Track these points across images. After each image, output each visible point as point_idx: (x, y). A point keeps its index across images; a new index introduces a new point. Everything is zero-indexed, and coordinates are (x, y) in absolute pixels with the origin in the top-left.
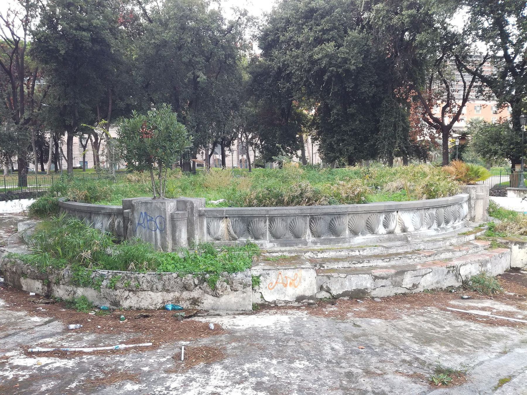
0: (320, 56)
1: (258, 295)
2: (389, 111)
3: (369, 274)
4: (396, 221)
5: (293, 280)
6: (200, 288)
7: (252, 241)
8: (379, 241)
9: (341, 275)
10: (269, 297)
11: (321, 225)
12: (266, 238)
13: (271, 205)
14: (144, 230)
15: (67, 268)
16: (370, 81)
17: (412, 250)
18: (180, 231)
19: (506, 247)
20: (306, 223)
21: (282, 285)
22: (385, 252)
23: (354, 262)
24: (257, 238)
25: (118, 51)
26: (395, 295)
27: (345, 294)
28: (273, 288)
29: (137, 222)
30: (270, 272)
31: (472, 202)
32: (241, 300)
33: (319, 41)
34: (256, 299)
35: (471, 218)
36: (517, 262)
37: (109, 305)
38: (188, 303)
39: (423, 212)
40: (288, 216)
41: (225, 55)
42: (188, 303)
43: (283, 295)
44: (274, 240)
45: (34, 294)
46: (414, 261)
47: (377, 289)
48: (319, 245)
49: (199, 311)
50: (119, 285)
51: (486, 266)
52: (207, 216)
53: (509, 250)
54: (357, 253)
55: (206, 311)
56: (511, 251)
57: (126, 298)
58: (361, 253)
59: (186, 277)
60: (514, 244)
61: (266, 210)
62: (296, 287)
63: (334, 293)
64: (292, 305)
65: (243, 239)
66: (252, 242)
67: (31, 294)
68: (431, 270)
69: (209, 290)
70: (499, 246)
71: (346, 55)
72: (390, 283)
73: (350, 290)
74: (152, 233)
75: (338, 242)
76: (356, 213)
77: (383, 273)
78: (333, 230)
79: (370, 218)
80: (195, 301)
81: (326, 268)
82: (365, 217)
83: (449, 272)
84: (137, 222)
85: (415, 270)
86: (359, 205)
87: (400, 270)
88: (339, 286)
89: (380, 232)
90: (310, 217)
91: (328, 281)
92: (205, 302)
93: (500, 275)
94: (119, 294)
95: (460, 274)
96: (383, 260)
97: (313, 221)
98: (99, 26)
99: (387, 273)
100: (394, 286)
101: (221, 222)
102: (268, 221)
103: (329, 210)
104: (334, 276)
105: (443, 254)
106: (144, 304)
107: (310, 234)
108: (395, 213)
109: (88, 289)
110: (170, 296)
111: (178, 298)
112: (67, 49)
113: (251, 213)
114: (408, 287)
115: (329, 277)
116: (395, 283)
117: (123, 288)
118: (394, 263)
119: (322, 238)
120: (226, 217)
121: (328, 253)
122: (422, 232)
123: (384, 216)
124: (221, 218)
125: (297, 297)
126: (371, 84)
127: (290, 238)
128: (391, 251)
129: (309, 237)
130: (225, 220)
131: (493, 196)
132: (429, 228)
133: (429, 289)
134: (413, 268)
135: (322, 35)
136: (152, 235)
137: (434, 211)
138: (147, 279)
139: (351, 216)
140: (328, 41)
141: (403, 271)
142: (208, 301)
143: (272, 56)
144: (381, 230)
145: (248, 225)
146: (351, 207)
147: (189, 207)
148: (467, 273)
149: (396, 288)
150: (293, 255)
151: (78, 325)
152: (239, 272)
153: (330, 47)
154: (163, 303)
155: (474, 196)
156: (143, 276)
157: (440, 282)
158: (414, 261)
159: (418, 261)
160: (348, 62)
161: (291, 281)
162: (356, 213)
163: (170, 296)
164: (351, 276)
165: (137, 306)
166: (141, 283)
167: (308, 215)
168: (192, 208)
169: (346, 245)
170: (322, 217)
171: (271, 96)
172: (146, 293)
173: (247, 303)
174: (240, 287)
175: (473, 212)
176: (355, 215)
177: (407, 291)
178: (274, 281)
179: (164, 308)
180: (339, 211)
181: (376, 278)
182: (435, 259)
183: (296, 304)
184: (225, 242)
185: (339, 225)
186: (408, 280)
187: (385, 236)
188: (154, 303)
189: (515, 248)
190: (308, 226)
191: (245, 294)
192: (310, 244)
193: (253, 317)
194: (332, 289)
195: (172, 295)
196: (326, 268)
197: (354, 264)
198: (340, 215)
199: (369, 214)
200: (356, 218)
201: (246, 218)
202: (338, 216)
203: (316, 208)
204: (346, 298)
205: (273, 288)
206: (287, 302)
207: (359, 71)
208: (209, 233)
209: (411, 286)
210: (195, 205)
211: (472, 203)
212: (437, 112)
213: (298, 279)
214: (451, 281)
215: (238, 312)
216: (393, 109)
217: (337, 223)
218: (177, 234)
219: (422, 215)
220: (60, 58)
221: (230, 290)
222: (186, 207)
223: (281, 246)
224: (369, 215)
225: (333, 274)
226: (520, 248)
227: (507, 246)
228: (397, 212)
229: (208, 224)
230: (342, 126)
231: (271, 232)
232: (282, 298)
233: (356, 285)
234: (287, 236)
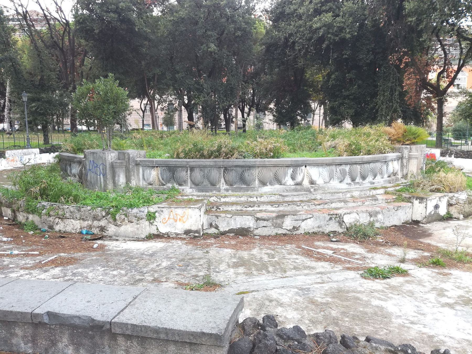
0: (318, 25)
1: (154, 228)
2: (387, 77)
3: (252, 216)
4: (303, 174)
5: (181, 217)
6: (106, 219)
7: (176, 186)
8: (286, 191)
9: (228, 215)
10: (163, 230)
11: (232, 176)
12: (188, 185)
13: (196, 158)
14: (92, 175)
15: (24, 199)
16: (368, 49)
17: (308, 199)
18: (119, 176)
19: (408, 202)
20: (220, 174)
21: (173, 220)
22: (281, 199)
23: (246, 206)
24: (180, 185)
25: (142, 29)
26: (275, 234)
27: (231, 231)
28: (166, 222)
29: (88, 168)
30: (163, 209)
31: (405, 161)
32: (136, 229)
33: (318, 12)
34: (153, 230)
35: (403, 176)
36: (417, 216)
37: (47, 228)
38: (98, 229)
39: (333, 167)
40: (205, 167)
41: (235, 29)
42: (98, 229)
43: (174, 229)
44: (194, 186)
45: (7, 218)
46: (302, 208)
47: (259, 229)
48: (230, 192)
49: (106, 237)
50: (52, 213)
51: (376, 216)
52: (142, 165)
53: (410, 204)
54: (255, 199)
55: (110, 237)
56: (413, 205)
57: (57, 224)
58: (259, 199)
59: (97, 210)
60: (415, 199)
61: (186, 161)
62: (184, 222)
63: (222, 230)
64: (181, 236)
65: (170, 185)
66: (177, 187)
67: (5, 218)
68: (311, 216)
69: (111, 220)
70: (403, 201)
71: (342, 25)
72: (271, 225)
73: (235, 228)
74: (98, 177)
75: (248, 191)
76: (264, 166)
77: (265, 216)
78: (242, 180)
79: (277, 171)
80: (102, 229)
81: (222, 210)
82: (274, 170)
83: (331, 219)
84: (88, 168)
85: (295, 215)
86: (266, 159)
87: (282, 213)
88: (226, 225)
89: (288, 184)
90: (224, 168)
91: (217, 220)
92: (109, 229)
93: (395, 226)
94: (52, 220)
95: (344, 222)
96: (272, 205)
97: (226, 172)
98: (124, 8)
99: (268, 215)
100: (275, 227)
101: (153, 170)
102: (189, 171)
103: (239, 163)
104: (222, 216)
105: (333, 204)
106: (69, 229)
107: (224, 183)
108: (303, 168)
109: (35, 215)
110: (85, 224)
111: (91, 226)
112: (101, 29)
113: (174, 163)
114: (288, 228)
115: (217, 217)
116: (276, 224)
117: (54, 216)
118: (283, 209)
119: (235, 186)
120: (157, 167)
121: (230, 198)
122: (331, 185)
123: (292, 170)
124: (153, 167)
125: (185, 231)
126: (368, 52)
127: (207, 185)
128: (287, 199)
129: (223, 186)
130: (156, 168)
131: (462, 158)
132: (341, 182)
133: (310, 232)
134: (294, 213)
135: (321, 7)
136: (98, 179)
137: (347, 168)
138: (70, 210)
139: (260, 169)
140: (327, 11)
141: (283, 215)
142: (112, 229)
143: (279, 27)
144: (289, 181)
145: (174, 174)
146: (258, 160)
147: (127, 157)
148: (352, 220)
149: (277, 229)
150: (200, 198)
151: (10, 239)
152: (136, 208)
153: (327, 17)
154: (81, 228)
155: (407, 156)
156: (68, 208)
157: (321, 227)
158: (302, 208)
159: (307, 208)
160: (344, 31)
161: (181, 218)
162: (264, 166)
163: (85, 224)
164: (236, 216)
165: (64, 230)
166: (65, 212)
167: (222, 166)
168: (129, 158)
169: (255, 193)
170: (234, 168)
171: (280, 64)
172: (69, 220)
173: (140, 233)
174: (134, 220)
175: (405, 170)
176: (264, 168)
177: (288, 232)
178: (167, 217)
179: (81, 233)
180: (248, 164)
181: (258, 219)
182: (324, 207)
183: (184, 236)
184: (155, 186)
185: (248, 176)
186: (288, 223)
187: (292, 187)
188: (75, 228)
189: (416, 202)
190: (222, 176)
191: (139, 225)
192: (222, 191)
193: (145, 243)
194: (220, 226)
195: (86, 222)
196: (222, 210)
197: (246, 207)
198: (250, 167)
199: (277, 167)
200: (265, 171)
201: (172, 168)
202: (248, 168)
203: (233, 161)
204: (232, 235)
205: (166, 222)
206: (177, 234)
207: (356, 39)
208: (144, 179)
209: (291, 228)
210: (131, 156)
211: (404, 162)
212: (432, 76)
213: (186, 216)
214: (333, 226)
215: (133, 239)
216: (391, 75)
217: (246, 174)
218: (116, 178)
219: (333, 171)
220: (96, 36)
221: (127, 221)
222: (125, 157)
223: (198, 192)
224: (277, 168)
225: (221, 215)
226: (420, 203)
227: (410, 200)
228: (306, 166)
229: (143, 171)
230: (343, 90)
231: (191, 180)
232: (173, 231)
233: (241, 224)
234: (205, 183)
